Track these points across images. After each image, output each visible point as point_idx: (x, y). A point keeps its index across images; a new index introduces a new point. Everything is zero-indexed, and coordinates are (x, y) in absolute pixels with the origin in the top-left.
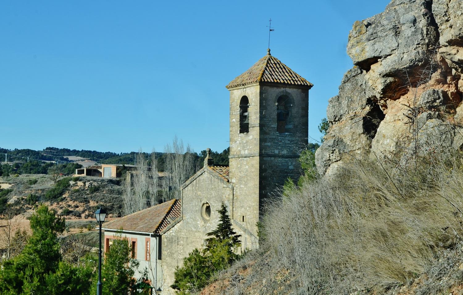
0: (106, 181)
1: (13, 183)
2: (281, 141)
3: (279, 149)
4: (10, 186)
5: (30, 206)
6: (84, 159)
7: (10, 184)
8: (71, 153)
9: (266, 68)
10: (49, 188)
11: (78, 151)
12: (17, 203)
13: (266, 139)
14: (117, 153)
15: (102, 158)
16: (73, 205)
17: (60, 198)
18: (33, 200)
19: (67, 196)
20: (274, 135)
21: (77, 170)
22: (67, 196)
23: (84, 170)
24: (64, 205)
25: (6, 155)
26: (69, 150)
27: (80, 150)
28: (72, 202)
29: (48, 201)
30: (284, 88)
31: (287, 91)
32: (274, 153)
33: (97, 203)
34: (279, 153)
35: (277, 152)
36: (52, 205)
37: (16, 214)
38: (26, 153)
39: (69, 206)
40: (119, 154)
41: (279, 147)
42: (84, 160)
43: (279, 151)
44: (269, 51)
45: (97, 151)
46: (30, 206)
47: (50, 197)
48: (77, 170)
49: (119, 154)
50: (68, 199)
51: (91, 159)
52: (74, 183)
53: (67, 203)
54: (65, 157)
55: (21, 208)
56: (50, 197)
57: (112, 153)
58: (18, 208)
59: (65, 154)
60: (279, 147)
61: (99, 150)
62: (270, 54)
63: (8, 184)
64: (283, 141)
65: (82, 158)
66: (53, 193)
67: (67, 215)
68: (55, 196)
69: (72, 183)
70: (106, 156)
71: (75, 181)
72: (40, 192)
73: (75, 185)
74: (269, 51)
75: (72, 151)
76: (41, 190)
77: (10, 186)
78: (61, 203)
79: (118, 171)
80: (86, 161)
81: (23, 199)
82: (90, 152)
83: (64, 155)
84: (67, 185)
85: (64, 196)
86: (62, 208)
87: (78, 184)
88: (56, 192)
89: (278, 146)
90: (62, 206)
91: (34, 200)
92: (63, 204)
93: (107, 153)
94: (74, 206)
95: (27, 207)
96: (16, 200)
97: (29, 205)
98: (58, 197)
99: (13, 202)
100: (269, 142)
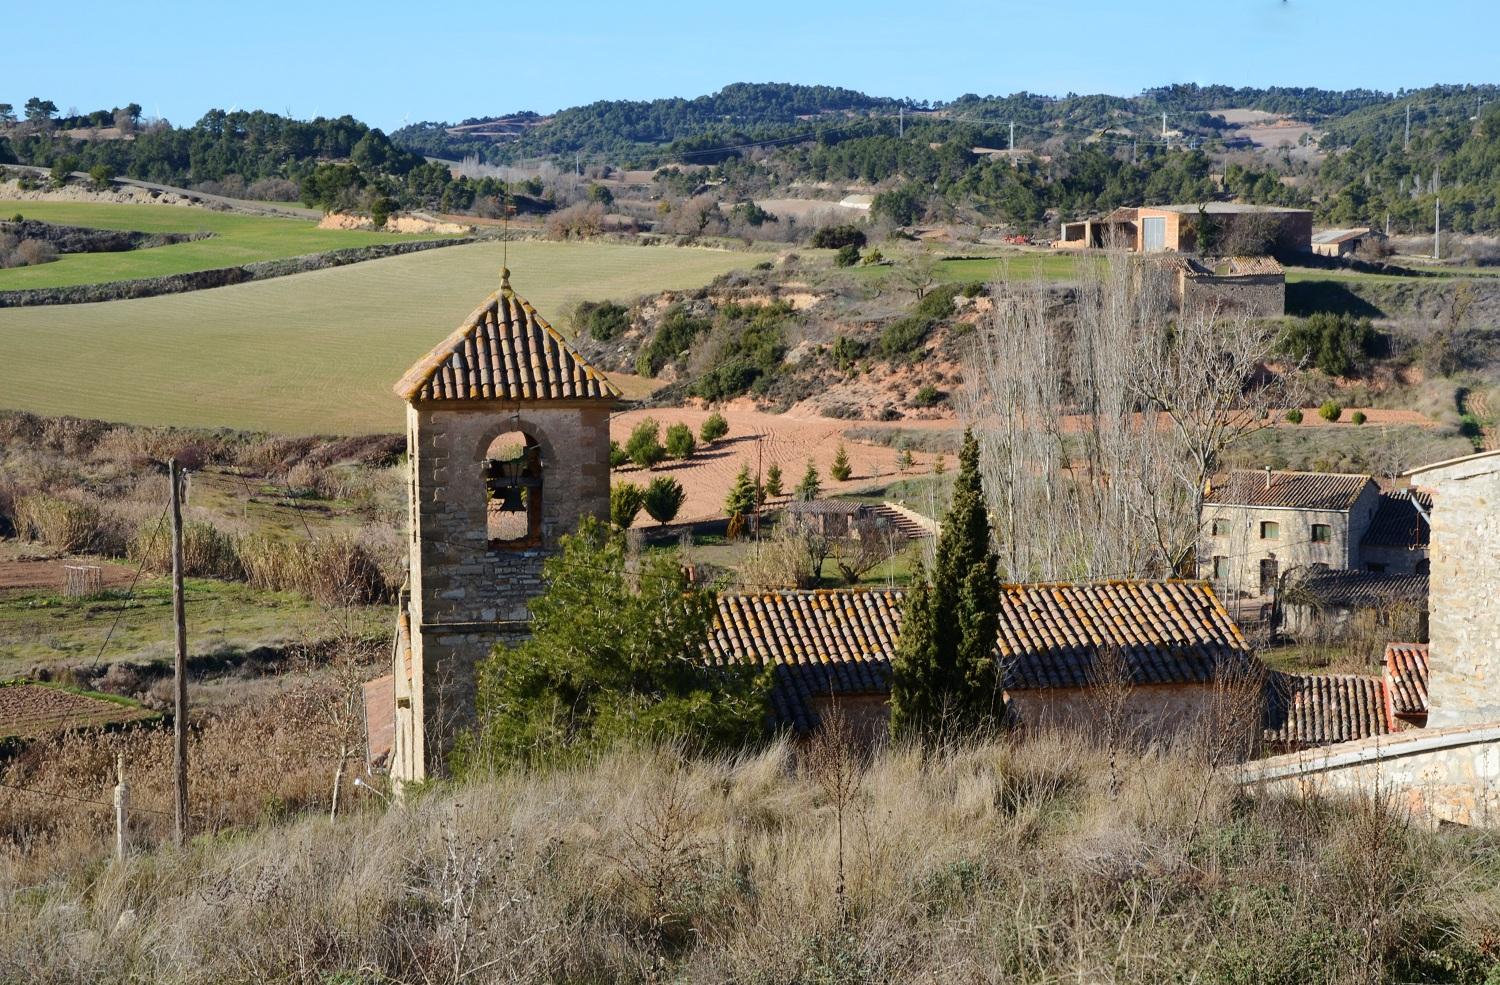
0: (1062, 293)
1: (825, 293)
2: (505, 582)
3: (497, 606)
4: (815, 300)
5: (838, 374)
6: (1274, 116)
7: (816, 295)
8: (1234, 99)
9: (451, 355)
10: (895, 318)
11: (1259, 93)
12: (808, 362)
13: (449, 577)
14: (1386, 91)
15: (1331, 111)
16: (950, 375)
17: (917, 351)
18: (845, 356)
19: (936, 346)
20: (477, 563)
21: (1063, 227)
22: (936, 346)
23: (1084, 226)
24: (927, 374)
25: (1012, 126)
26: (1231, 89)
27: (1265, 87)
28: (947, 365)
29: (884, 358)
30: (510, 410)
31: (523, 418)
32: (479, 619)
33: (1178, 309)
34: (498, 619)
35: (488, 615)
36: (894, 372)
37: (801, 399)
38: (1095, 106)
39: (940, 377)
40: (1391, 95)
41: (498, 601)
42: (1275, 121)
43: (498, 614)
44: (507, 274)
45: (1321, 87)
46: (838, 374)
47: (890, 347)
48: (1063, 227)
49: (1391, 95)
50: (941, 355)
51: (1295, 118)
52: (966, 300)
53: (936, 370)
54: (1214, 114)
55: (816, 377)
56: (890, 347)
57: (1368, 93)
58: (808, 377)
59: (1216, 102)
60: (498, 601)
61: (1325, 84)
62: (507, 287)
63: (809, 297)
64: (513, 580)
65: (1268, 115)
66: (898, 334)
67: (929, 407)
68: (905, 344)
69: (960, 300)
70: (1348, 103)
71: (970, 295)
72: (870, 330)
73: (970, 308)
74: (507, 274)
75: (1237, 93)
76: (874, 322)
77: (815, 300)
78: (918, 368)
79: (1185, 229)
80: (1281, 123)
81: (822, 351)
82: (1297, 92)
83: (1211, 108)
84: (946, 308)
85: (929, 345)
86: (919, 383)
87: (978, 306)
88: (907, 334)
89: (494, 597)
90: (919, 377)
91: (850, 355)
92: (924, 370)
93: (1352, 93)
94: (953, 377)
95: (831, 376)
96: (806, 352)
97: (837, 369)
98: (912, 349)
99: (797, 360)
100: (458, 588)
